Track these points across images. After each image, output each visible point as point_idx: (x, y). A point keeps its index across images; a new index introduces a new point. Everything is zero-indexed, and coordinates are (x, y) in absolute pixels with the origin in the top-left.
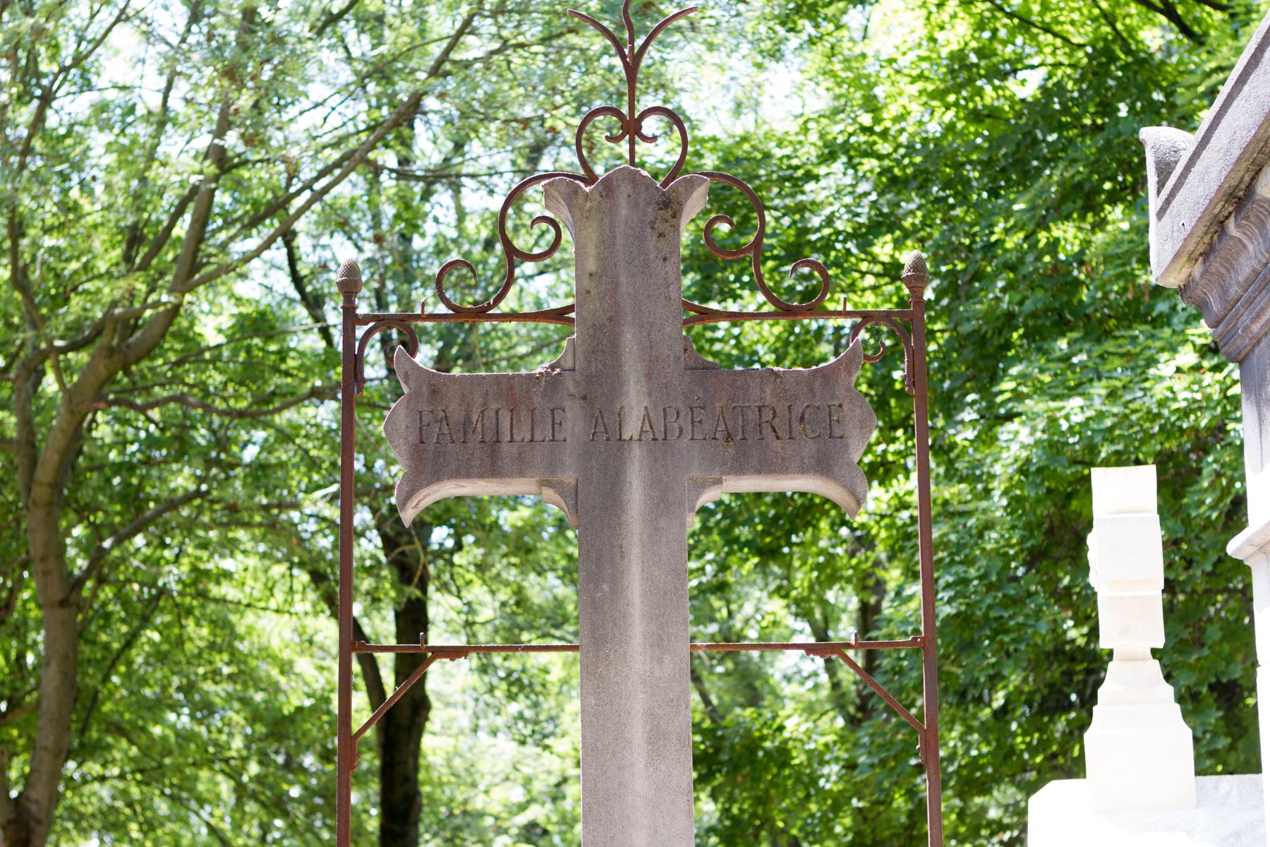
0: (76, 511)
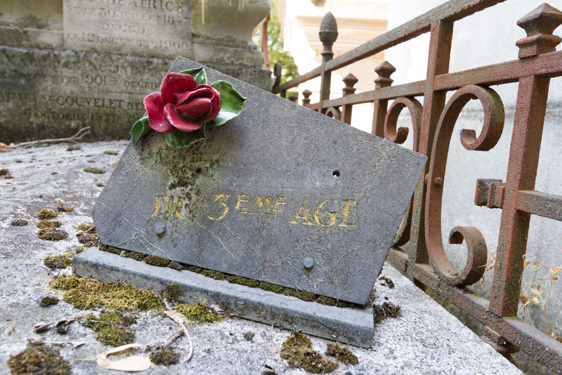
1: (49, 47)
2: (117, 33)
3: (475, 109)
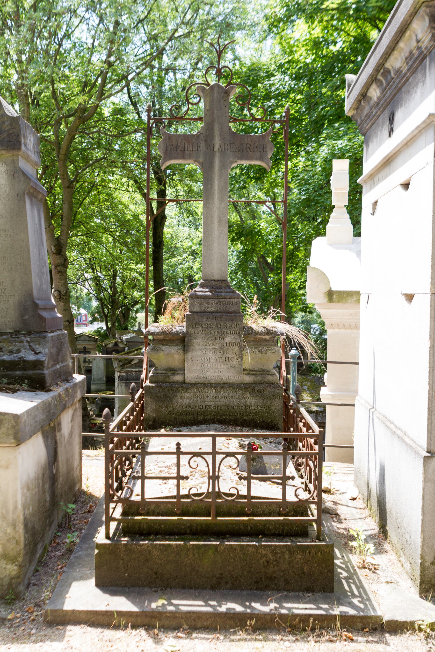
0: (70, 162)
2: (208, 374)
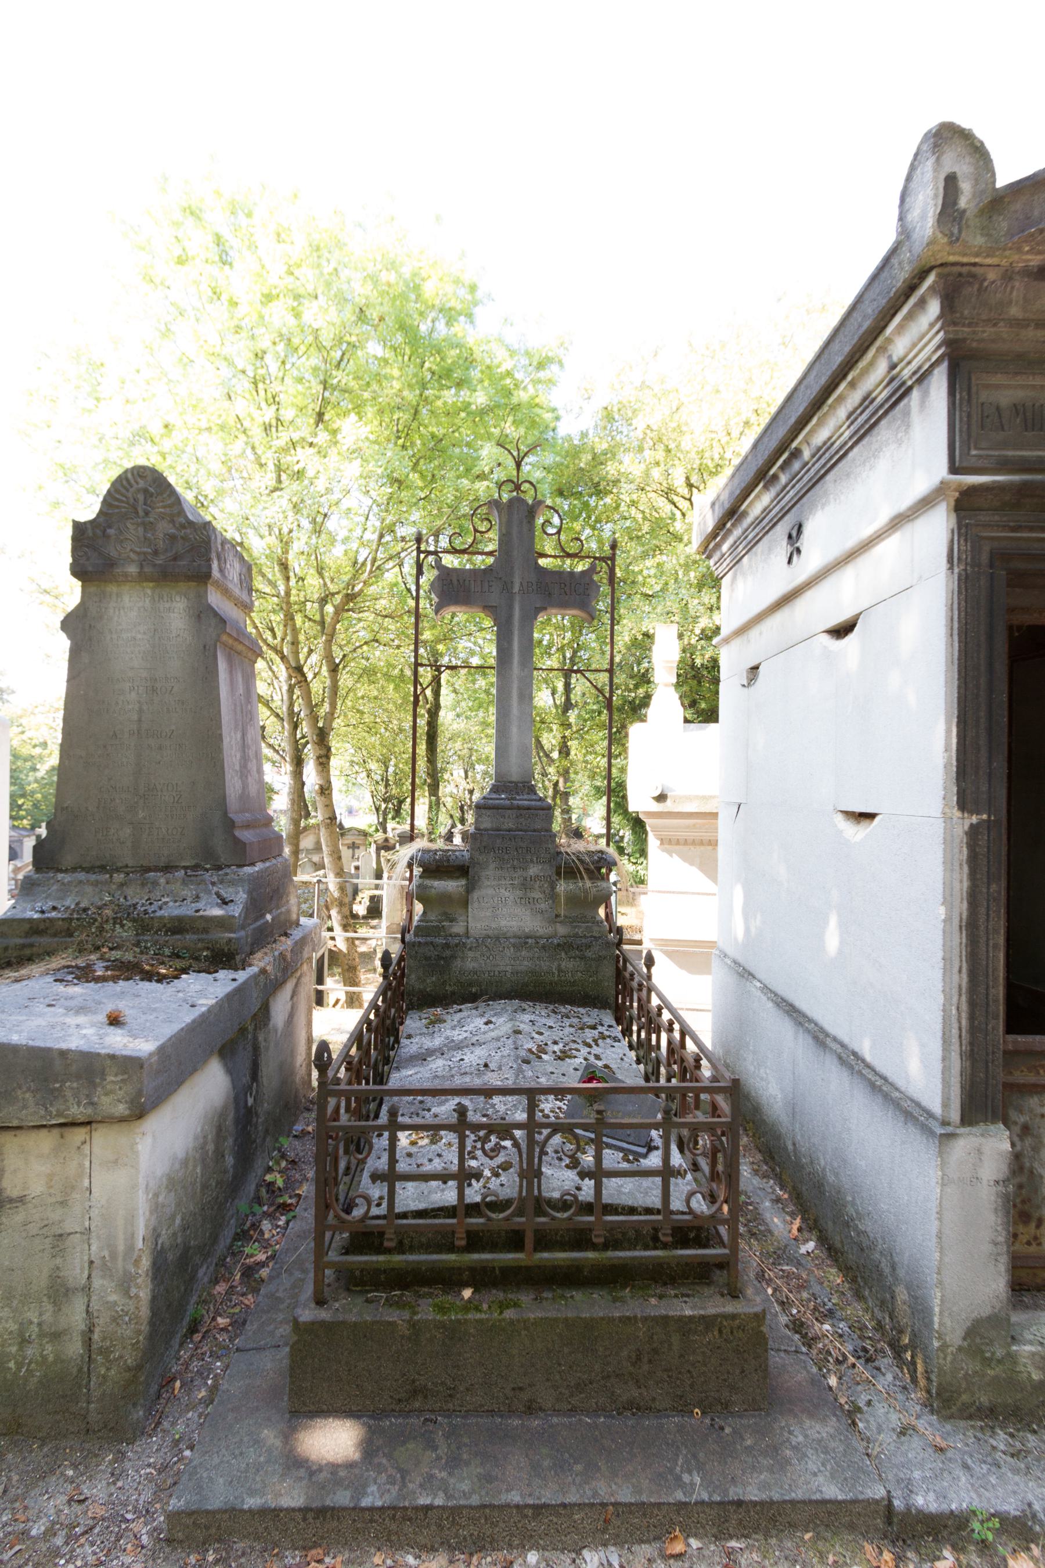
1: (457, 935)
2: (503, 923)
3: (835, 1061)
